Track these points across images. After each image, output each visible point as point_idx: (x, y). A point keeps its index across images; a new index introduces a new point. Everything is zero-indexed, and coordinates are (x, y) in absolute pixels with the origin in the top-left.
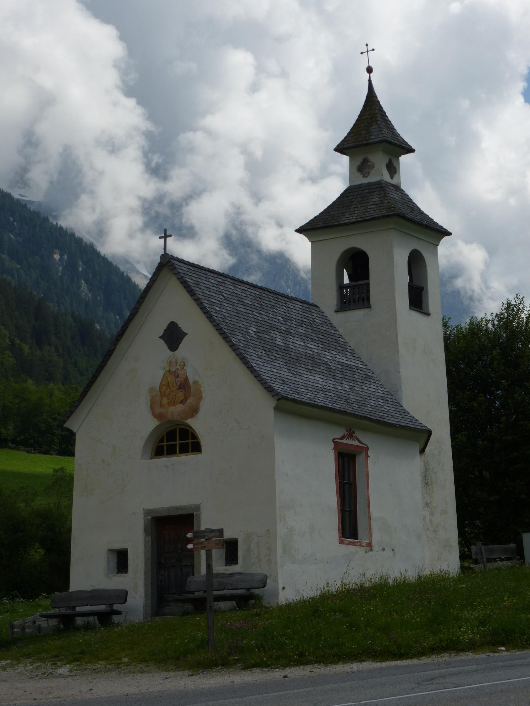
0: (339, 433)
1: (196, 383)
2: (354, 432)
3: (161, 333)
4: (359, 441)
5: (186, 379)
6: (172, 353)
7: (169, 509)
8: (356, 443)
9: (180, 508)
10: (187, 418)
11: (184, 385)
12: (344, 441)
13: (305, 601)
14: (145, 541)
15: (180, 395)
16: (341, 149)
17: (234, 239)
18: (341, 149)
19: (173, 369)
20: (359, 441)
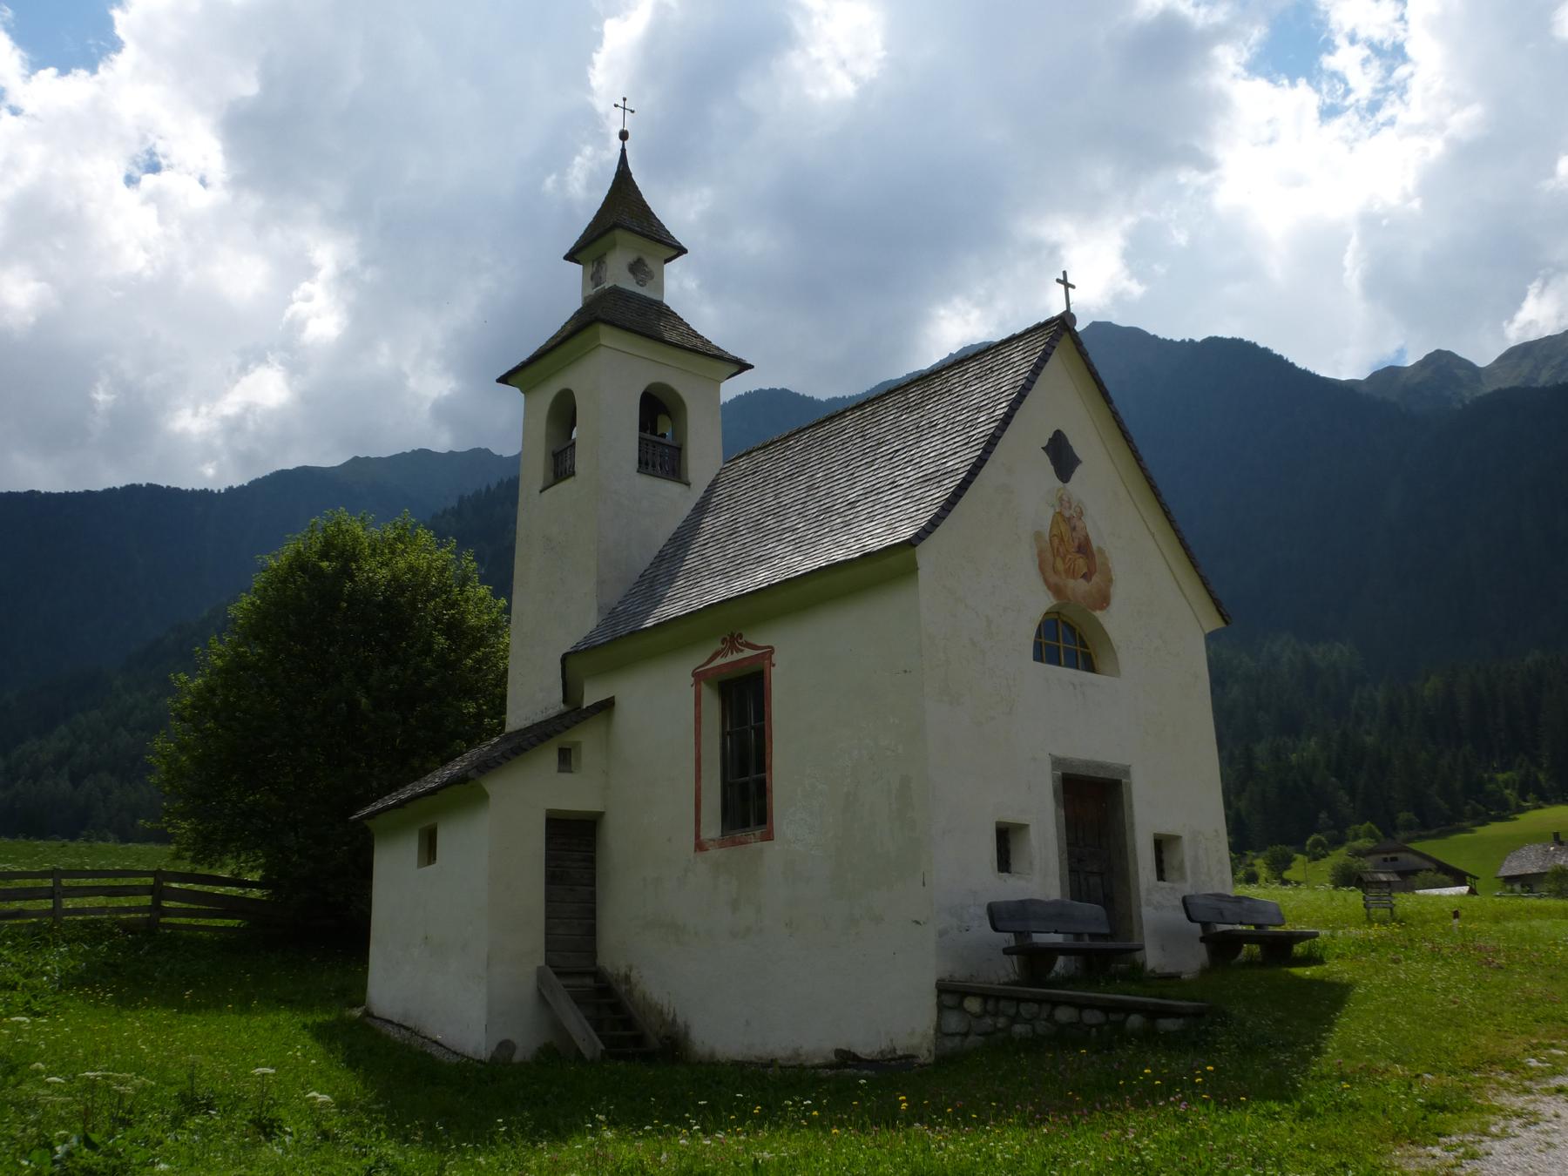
0: (698, 659)
1: (1100, 550)
2: (740, 636)
3: (1045, 444)
4: (755, 647)
5: (1087, 538)
6: (1060, 484)
7: (1087, 764)
8: (748, 653)
9: (1101, 766)
10: (1095, 609)
11: (1084, 548)
12: (720, 661)
13: (802, 1067)
14: (1057, 817)
15: (1081, 562)
16: (571, 256)
17: (1013, 943)
18: (571, 256)
19: (1067, 514)
20: (755, 647)
